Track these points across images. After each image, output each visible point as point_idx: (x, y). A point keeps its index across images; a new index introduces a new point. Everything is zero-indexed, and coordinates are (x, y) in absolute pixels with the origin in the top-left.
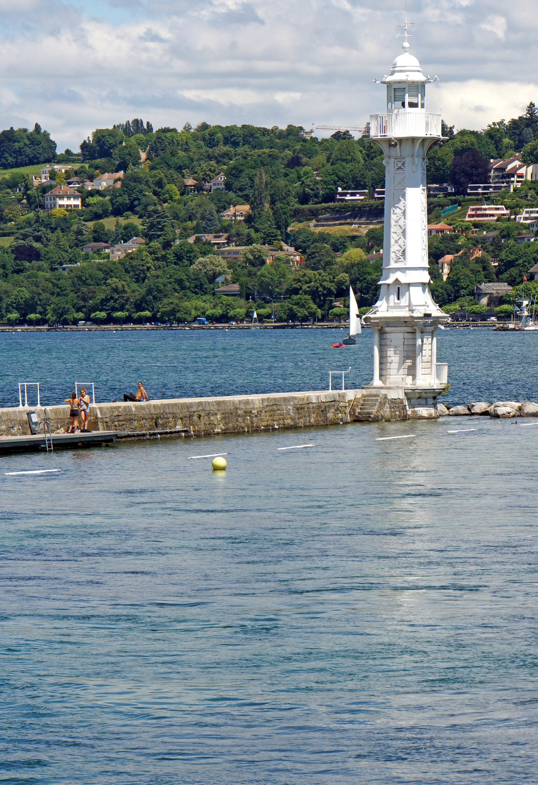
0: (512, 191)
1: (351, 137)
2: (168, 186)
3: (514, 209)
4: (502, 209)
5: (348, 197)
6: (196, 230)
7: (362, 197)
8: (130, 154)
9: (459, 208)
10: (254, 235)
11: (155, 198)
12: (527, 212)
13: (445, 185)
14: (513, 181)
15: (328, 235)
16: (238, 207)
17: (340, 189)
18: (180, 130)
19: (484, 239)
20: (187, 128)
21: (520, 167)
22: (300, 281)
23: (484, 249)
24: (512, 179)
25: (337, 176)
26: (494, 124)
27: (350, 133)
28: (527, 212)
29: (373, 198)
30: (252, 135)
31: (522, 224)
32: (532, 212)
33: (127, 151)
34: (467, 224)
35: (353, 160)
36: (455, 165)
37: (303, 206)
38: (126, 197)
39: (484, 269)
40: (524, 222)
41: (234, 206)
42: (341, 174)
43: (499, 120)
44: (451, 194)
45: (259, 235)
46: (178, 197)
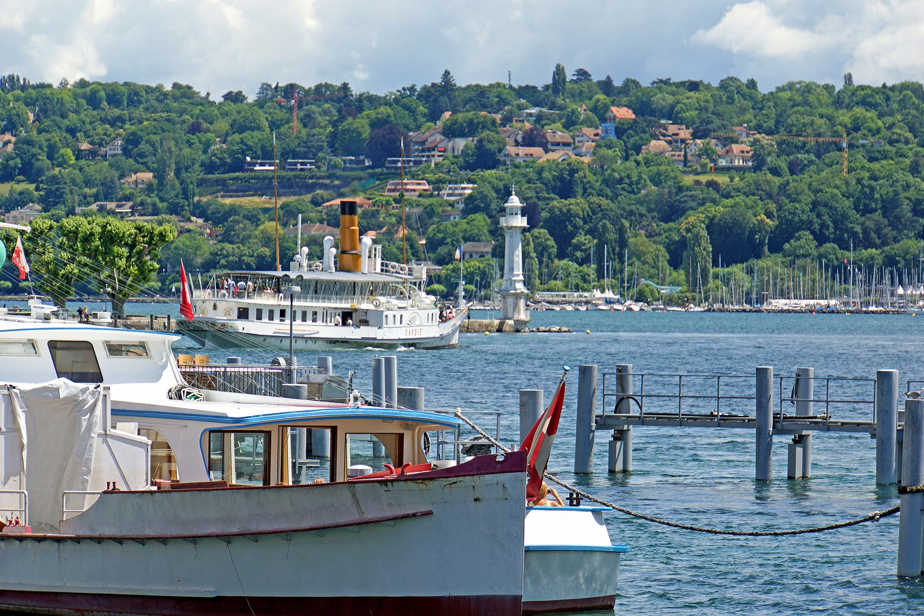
0: (433, 165)
1: (244, 98)
2: (62, 151)
3: (438, 184)
4: (424, 184)
5: (257, 168)
6: (96, 198)
7: (273, 168)
8: (18, 115)
9: (378, 182)
10: (160, 205)
11: (49, 162)
12: (450, 188)
13: (362, 157)
14: (434, 156)
15: (240, 206)
16: (139, 174)
17: (248, 159)
18: (56, 85)
19: (409, 217)
20: (64, 84)
21: (441, 141)
22: (218, 255)
23: (410, 227)
24: (433, 153)
25: (246, 145)
26: (404, 89)
27: (244, 93)
28: (450, 188)
29: (284, 169)
30: (137, 94)
31: (446, 201)
32: (456, 189)
33: (14, 112)
34: (387, 198)
35: (259, 128)
36: (372, 138)
37: (210, 176)
38: (18, 160)
39: (412, 247)
40: (448, 198)
41: (135, 173)
42: (250, 143)
43: (410, 86)
44: (368, 167)
45: (165, 204)
46: (73, 162)
